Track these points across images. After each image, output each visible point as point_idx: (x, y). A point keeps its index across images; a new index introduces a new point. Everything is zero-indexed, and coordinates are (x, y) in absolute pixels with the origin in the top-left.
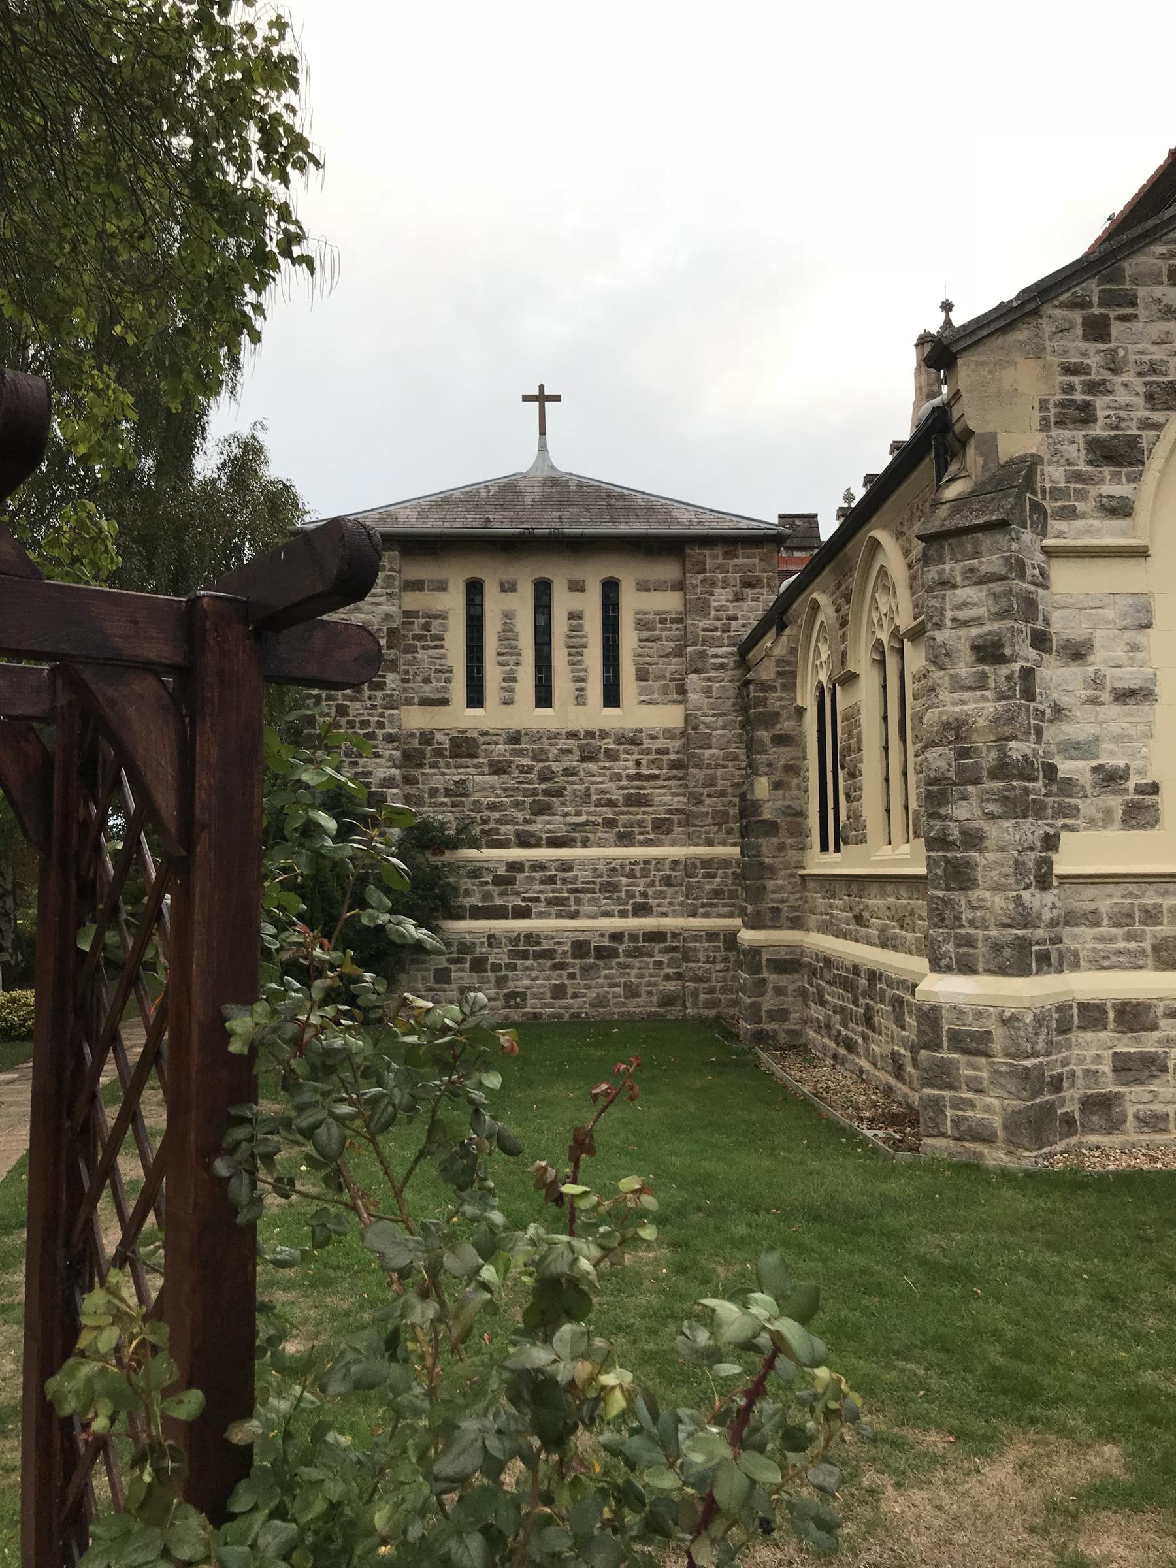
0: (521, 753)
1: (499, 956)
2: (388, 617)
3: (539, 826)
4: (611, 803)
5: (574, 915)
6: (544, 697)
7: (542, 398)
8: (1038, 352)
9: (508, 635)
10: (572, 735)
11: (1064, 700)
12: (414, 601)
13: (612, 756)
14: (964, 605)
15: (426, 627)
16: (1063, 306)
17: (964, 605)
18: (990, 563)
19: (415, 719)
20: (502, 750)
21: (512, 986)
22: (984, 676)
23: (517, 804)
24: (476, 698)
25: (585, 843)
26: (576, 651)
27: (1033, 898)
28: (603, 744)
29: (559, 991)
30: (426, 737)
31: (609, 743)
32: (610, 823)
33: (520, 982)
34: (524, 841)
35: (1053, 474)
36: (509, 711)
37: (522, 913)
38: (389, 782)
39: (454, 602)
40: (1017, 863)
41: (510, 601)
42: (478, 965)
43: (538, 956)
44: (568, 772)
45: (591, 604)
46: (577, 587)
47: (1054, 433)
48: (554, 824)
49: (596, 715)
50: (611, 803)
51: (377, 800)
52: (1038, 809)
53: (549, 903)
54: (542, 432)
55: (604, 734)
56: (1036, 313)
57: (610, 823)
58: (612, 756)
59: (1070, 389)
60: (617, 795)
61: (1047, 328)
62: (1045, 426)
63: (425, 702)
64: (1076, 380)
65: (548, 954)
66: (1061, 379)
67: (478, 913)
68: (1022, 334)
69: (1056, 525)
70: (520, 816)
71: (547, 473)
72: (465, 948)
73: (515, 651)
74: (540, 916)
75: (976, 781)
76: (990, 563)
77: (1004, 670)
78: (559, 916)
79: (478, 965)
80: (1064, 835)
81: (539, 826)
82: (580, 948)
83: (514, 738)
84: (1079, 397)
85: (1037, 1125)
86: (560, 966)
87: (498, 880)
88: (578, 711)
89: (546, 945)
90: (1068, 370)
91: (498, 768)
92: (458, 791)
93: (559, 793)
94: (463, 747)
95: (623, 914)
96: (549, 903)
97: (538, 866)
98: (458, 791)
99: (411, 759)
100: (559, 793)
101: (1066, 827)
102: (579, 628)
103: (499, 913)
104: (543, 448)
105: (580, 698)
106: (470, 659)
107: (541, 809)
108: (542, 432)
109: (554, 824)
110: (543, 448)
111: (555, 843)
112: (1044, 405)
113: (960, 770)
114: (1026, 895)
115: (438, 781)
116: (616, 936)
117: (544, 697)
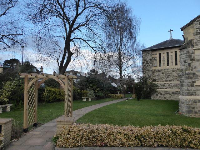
0: (165, 71)
1: (163, 93)
2: (150, 58)
3: (168, 79)
4: (176, 76)
5: (172, 89)
6: (168, 65)
7: (171, 31)
8: (193, 27)
9: (164, 58)
10: (171, 69)
11: (196, 66)
12: (153, 56)
13: (176, 71)
14: (183, 57)
15: (155, 59)
16: (196, 22)
17: (183, 57)
18: (185, 52)
19: (154, 68)
20: (163, 71)
21: (165, 96)
22: (185, 64)
23: (165, 77)
24: (160, 66)
25: (173, 81)
26: (172, 59)
27: (190, 88)
28: (175, 70)
29: (170, 97)
30: (155, 70)
31: (176, 70)
32: (176, 79)
33: (166, 96)
34: (166, 81)
35: (195, 41)
36: (164, 66)
37: (166, 89)
38: (151, 75)
39: (158, 56)
40: (187, 84)
41: (164, 55)
42: (161, 94)
43: (168, 93)
44: (171, 73)
45: (174, 54)
46: (172, 52)
47: (195, 36)
48: (169, 79)
49: (175, 66)
50: (176, 76)
51: (150, 77)
52: (191, 78)
53: (169, 88)
54: (171, 35)
55: (175, 69)
56: (193, 23)
57: (176, 79)
58: (176, 71)
59: (197, 31)
60: (177, 75)
61: (194, 24)
62: (194, 35)
63: (155, 66)
64: (198, 30)
65: (169, 93)
66: (196, 30)
67: (161, 88)
68: (191, 26)
69: (195, 46)
70: (165, 78)
71: (171, 39)
72: (159, 92)
73: (164, 60)
74: (168, 89)
75: (184, 75)
76: (185, 52)
77: (187, 63)
78: (170, 89)
79: (161, 94)
80: (197, 81)
81: (168, 79)
82: (173, 93)
83: (165, 70)
84: (198, 31)
85: (189, 112)
86: (170, 95)
87: (163, 85)
88: (172, 66)
89: (169, 92)
90: (197, 29)
91: (163, 73)
92: (158, 76)
93: (170, 75)
94: (159, 71)
95: (178, 89)
96: (169, 88)
97: (168, 84)
98: (158, 76)
99: (153, 72)
100: (170, 75)
101: (197, 80)
102: (172, 57)
103: (163, 89)
104: (171, 36)
105: (172, 65)
106: (161, 60)
107: (168, 77)
108: (171, 35)
109: (169, 79)
110: (171, 36)
111: (170, 81)
112: (194, 33)
113: (182, 74)
114: (188, 88)
115: (156, 75)
116: (177, 92)
117: (168, 65)
